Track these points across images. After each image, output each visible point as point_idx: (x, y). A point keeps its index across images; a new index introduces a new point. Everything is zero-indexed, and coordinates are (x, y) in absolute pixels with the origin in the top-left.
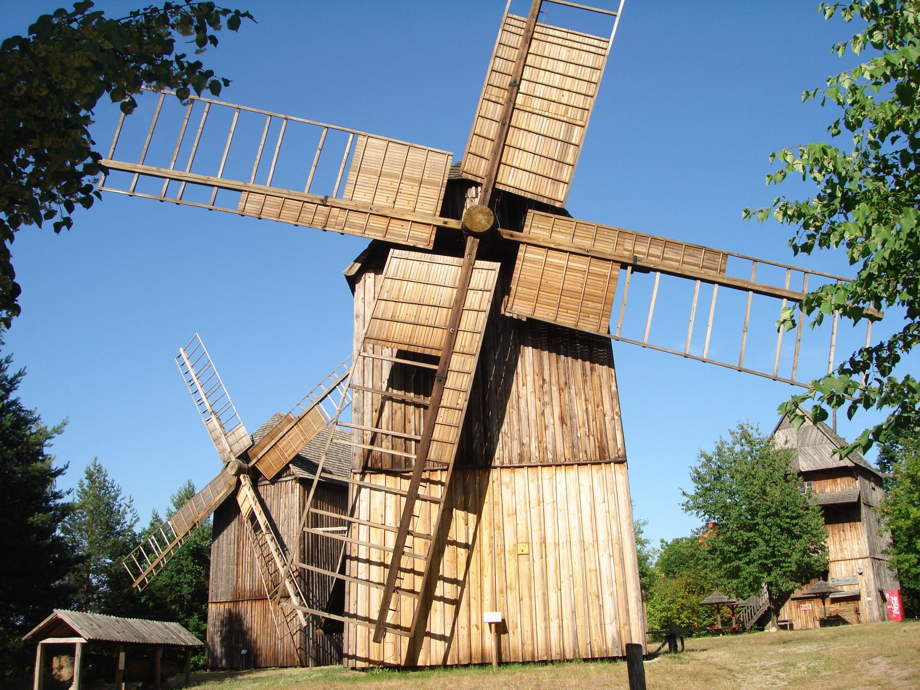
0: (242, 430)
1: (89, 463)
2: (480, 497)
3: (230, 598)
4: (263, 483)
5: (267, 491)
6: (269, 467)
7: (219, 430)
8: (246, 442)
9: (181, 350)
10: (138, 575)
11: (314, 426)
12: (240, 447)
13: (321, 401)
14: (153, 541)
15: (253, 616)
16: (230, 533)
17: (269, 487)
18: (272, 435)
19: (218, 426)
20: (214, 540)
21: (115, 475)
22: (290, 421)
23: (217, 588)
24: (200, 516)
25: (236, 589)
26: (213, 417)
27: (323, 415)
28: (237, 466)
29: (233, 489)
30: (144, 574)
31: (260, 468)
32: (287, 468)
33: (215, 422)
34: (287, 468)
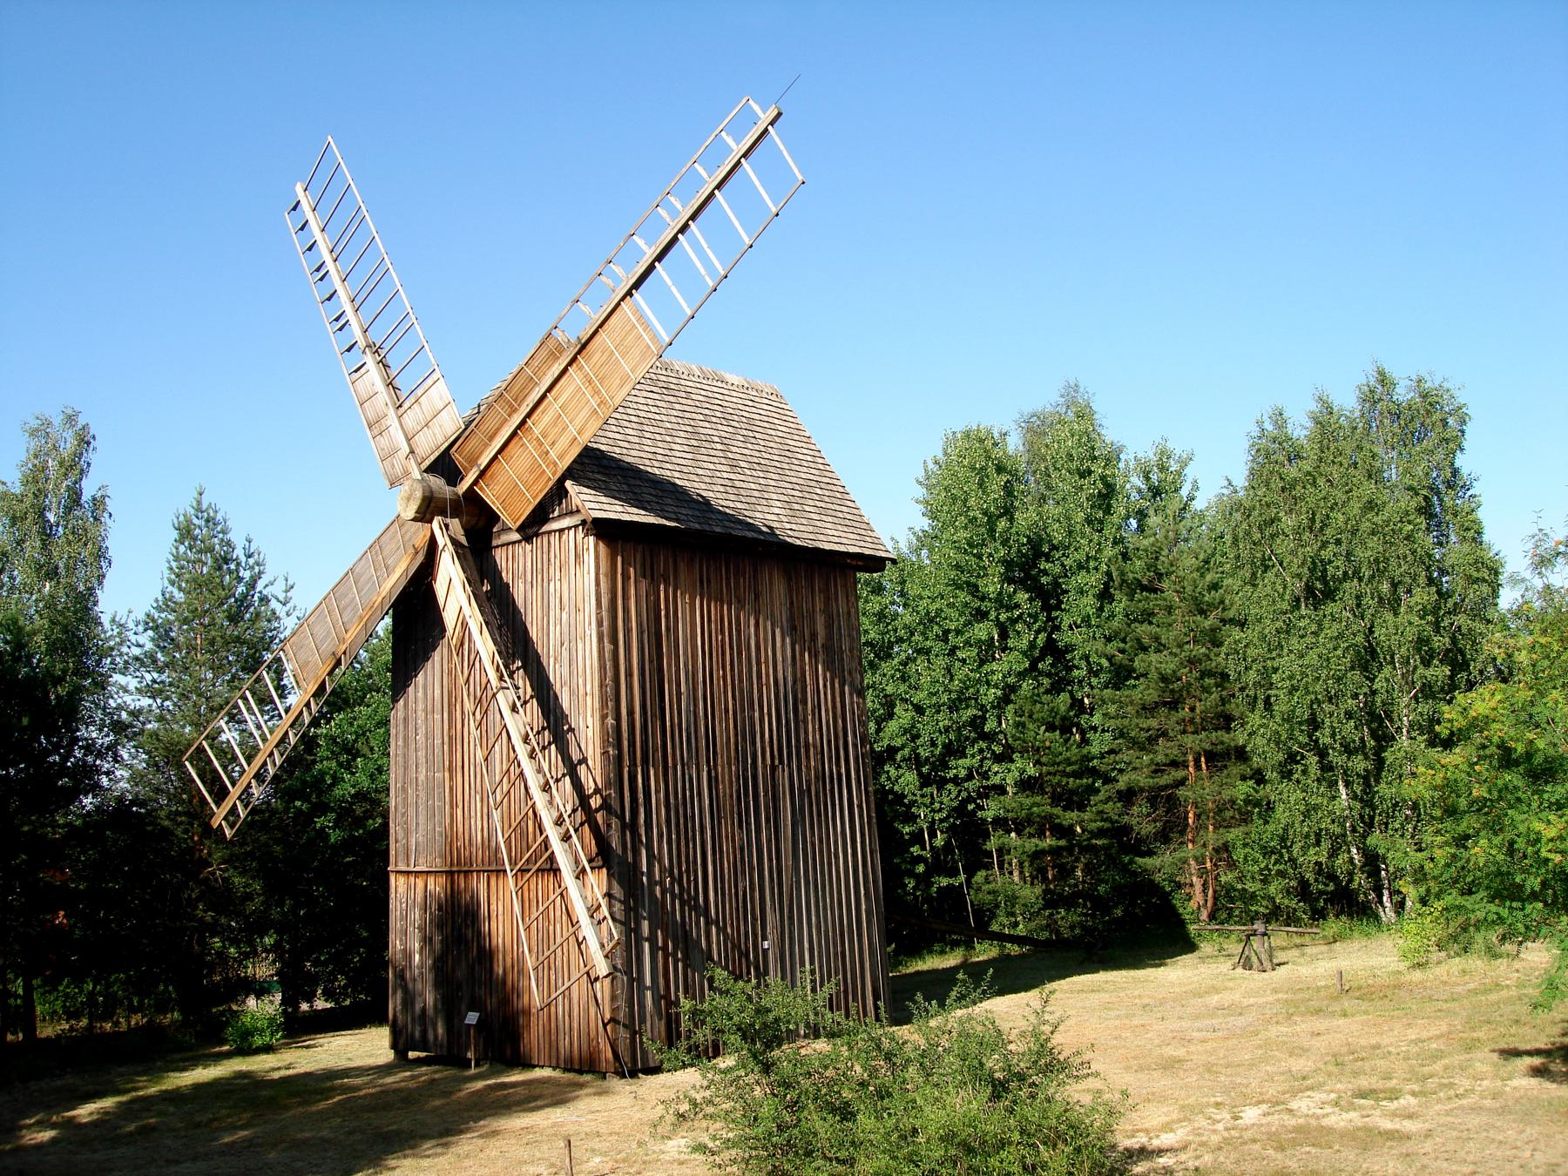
0: (439, 393)
1: (186, 505)
2: (619, 758)
3: (438, 865)
4: (505, 538)
5: (515, 561)
6: (511, 495)
7: (384, 395)
8: (448, 425)
9: (299, 189)
10: (221, 794)
11: (622, 362)
12: (431, 443)
13: (637, 285)
14: (249, 709)
15: (505, 912)
16: (430, 680)
17: (519, 549)
18: (518, 405)
19: (380, 386)
20: (395, 700)
21: (243, 529)
22: (560, 349)
23: (407, 833)
24: (350, 637)
25: (450, 839)
26: (370, 360)
27: (647, 326)
28: (419, 494)
29: (420, 558)
30: (234, 792)
31: (489, 495)
32: (558, 493)
33: (373, 376)
34: (558, 493)
